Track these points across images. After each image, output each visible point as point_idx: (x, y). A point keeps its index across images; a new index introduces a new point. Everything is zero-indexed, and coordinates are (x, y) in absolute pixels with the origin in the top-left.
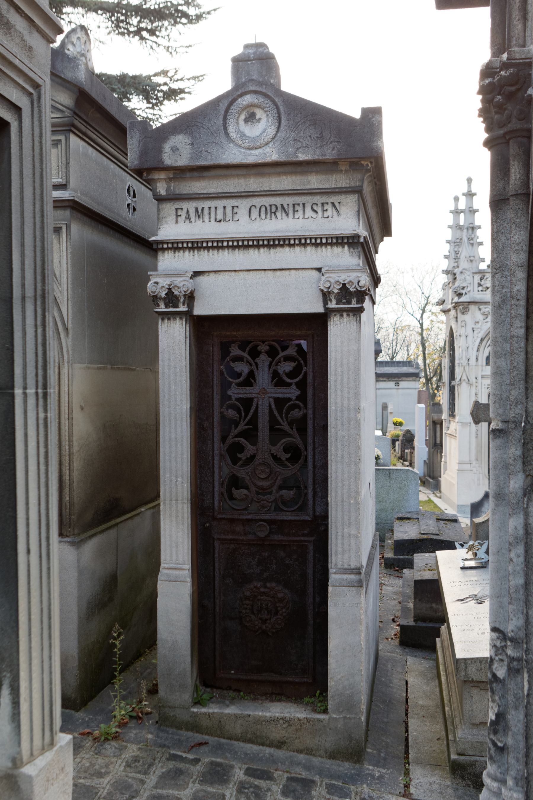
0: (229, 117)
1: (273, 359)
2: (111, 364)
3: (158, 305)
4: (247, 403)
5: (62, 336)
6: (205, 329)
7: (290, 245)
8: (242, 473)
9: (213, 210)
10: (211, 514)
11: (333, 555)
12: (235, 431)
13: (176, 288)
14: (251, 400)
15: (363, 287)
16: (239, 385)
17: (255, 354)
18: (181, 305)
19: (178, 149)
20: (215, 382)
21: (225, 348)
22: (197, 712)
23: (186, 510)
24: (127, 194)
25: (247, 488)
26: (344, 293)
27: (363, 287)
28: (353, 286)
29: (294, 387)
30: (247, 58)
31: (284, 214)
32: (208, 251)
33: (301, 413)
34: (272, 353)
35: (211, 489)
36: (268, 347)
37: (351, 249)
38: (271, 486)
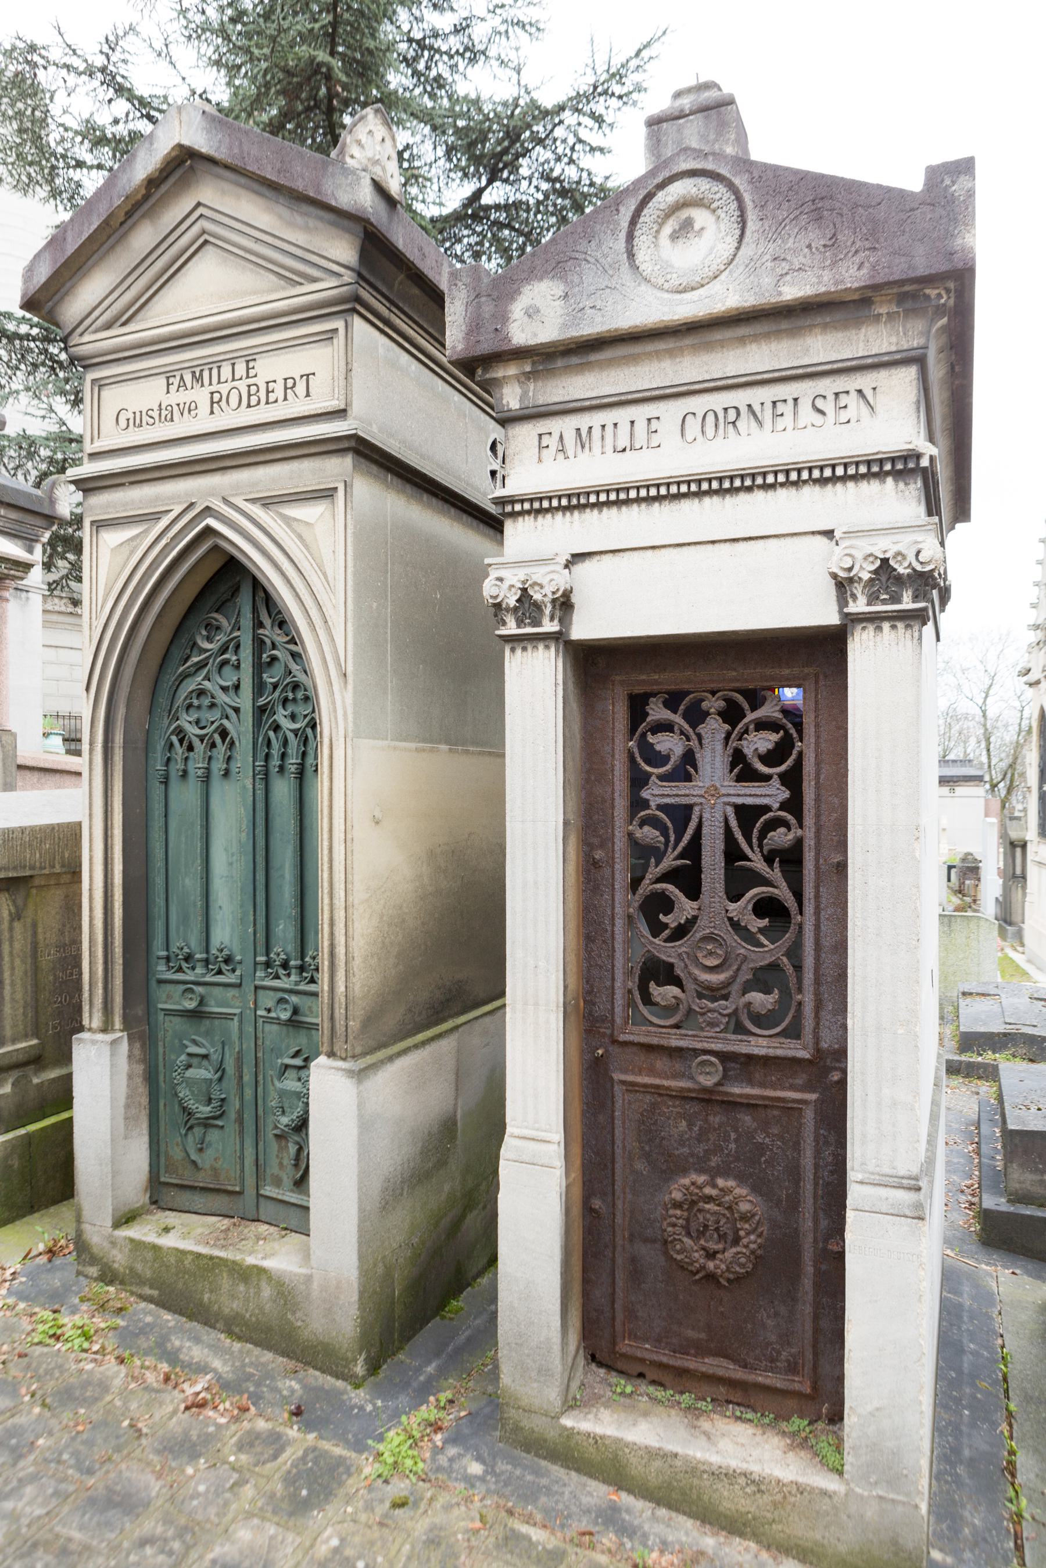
0: (636, 234)
1: (733, 729)
2: (447, 743)
3: (504, 623)
4: (681, 814)
5: (336, 687)
6: (595, 664)
7: (766, 487)
8: (668, 952)
9: (609, 429)
10: (608, 1032)
11: (857, 1143)
12: (655, 871)
13: (537, 588)
14: (689, 808)
15: (928, 563)
16: (662, 778)
17: (696, 716)
18: (546, 620)
19: (538, 311)
20: (617, 773)
21: (637, 707)
22: (573, 1428)
23: (553, 1026)
24: (489, 453)
25: (678, 983)
26: (884, 579)
27: (928, 563)
28: (906, 564)
29: (776, 782)
30: (677, 114)
31: (753, 423)
32: (600, 511)
33: (791, 836)
34: (731, 715)
35: (608, 983)
36: (722, 704)
37: (901, 485)
38: (727, 984)
